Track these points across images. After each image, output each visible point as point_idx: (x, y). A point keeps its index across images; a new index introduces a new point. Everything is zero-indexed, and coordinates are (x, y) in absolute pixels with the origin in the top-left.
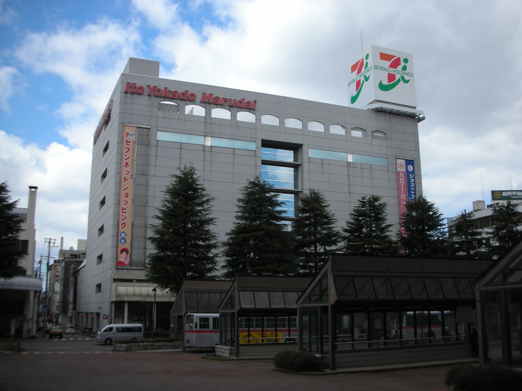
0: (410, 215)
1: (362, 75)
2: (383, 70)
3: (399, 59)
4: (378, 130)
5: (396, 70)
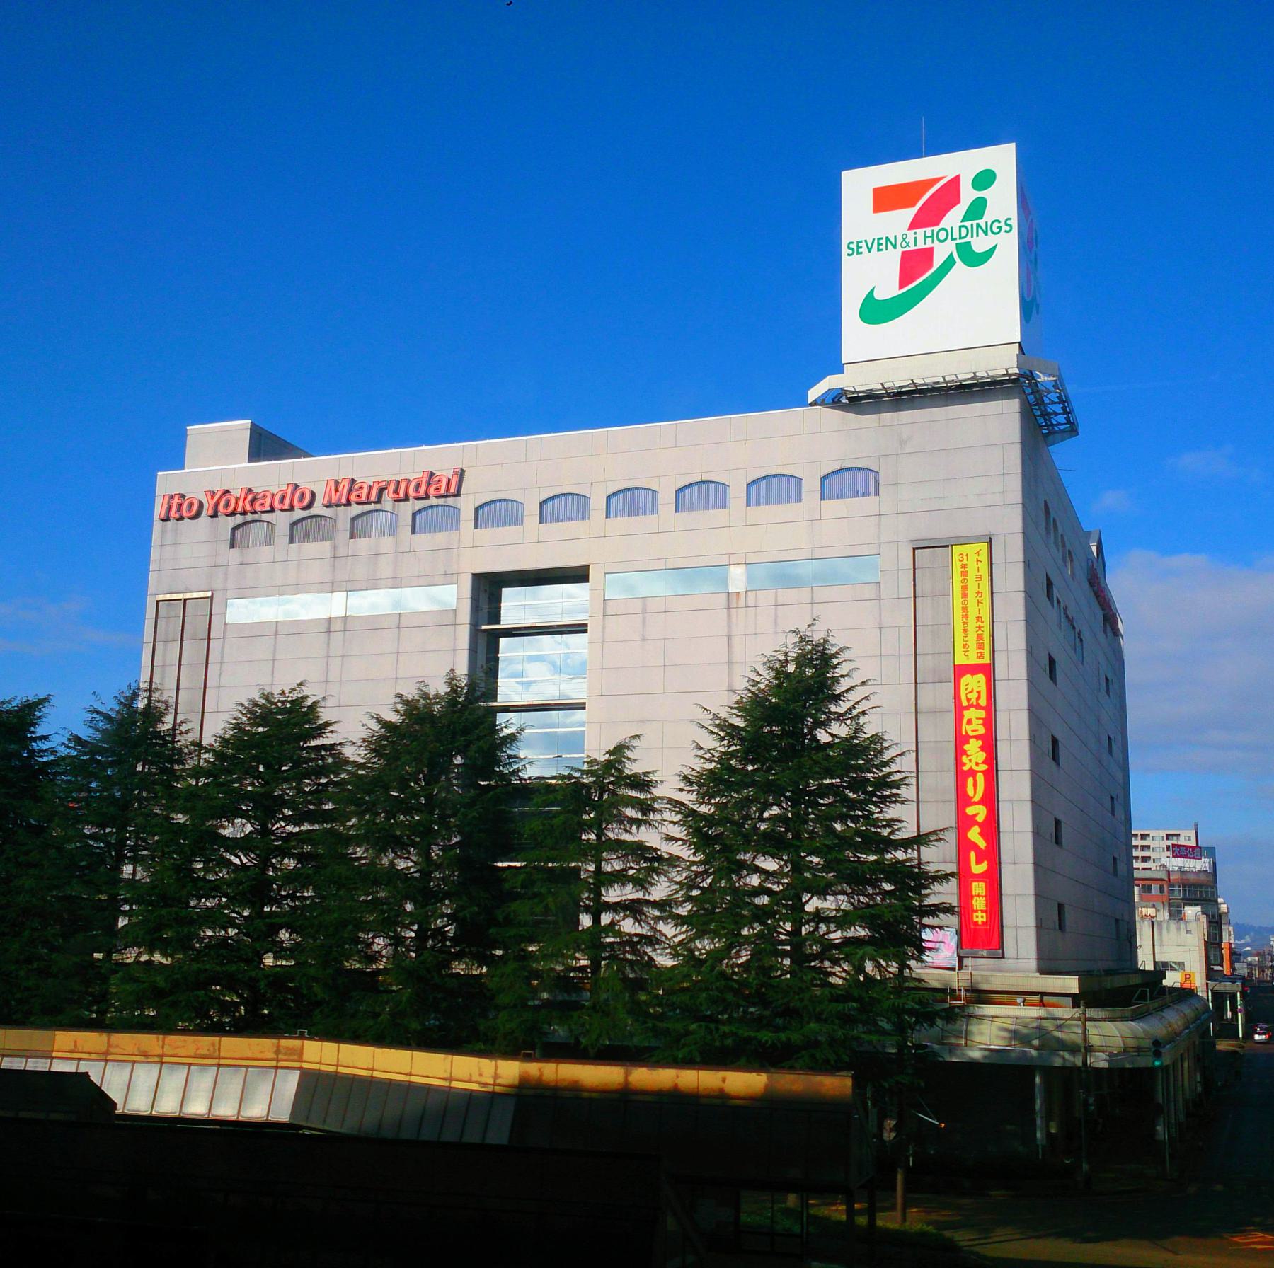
0: (852, 839)
1: (942, 235)
2: (883, 247)
3: (956, 181)
4: (846, 465)
5: (936, 229)
